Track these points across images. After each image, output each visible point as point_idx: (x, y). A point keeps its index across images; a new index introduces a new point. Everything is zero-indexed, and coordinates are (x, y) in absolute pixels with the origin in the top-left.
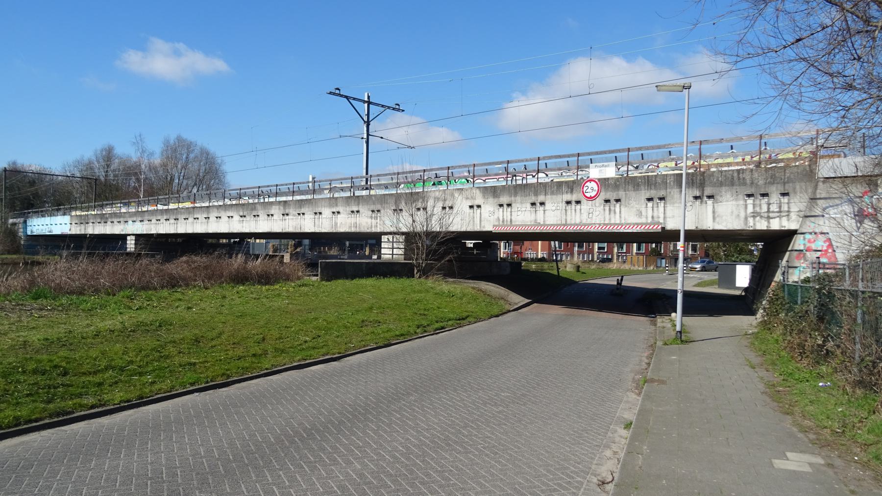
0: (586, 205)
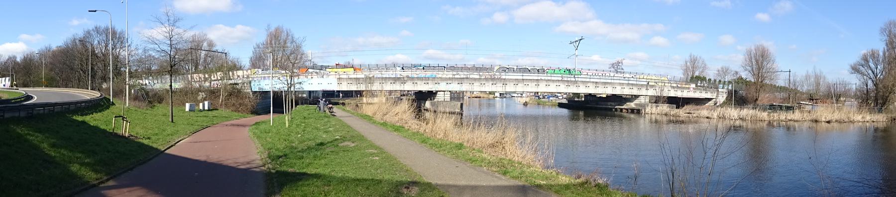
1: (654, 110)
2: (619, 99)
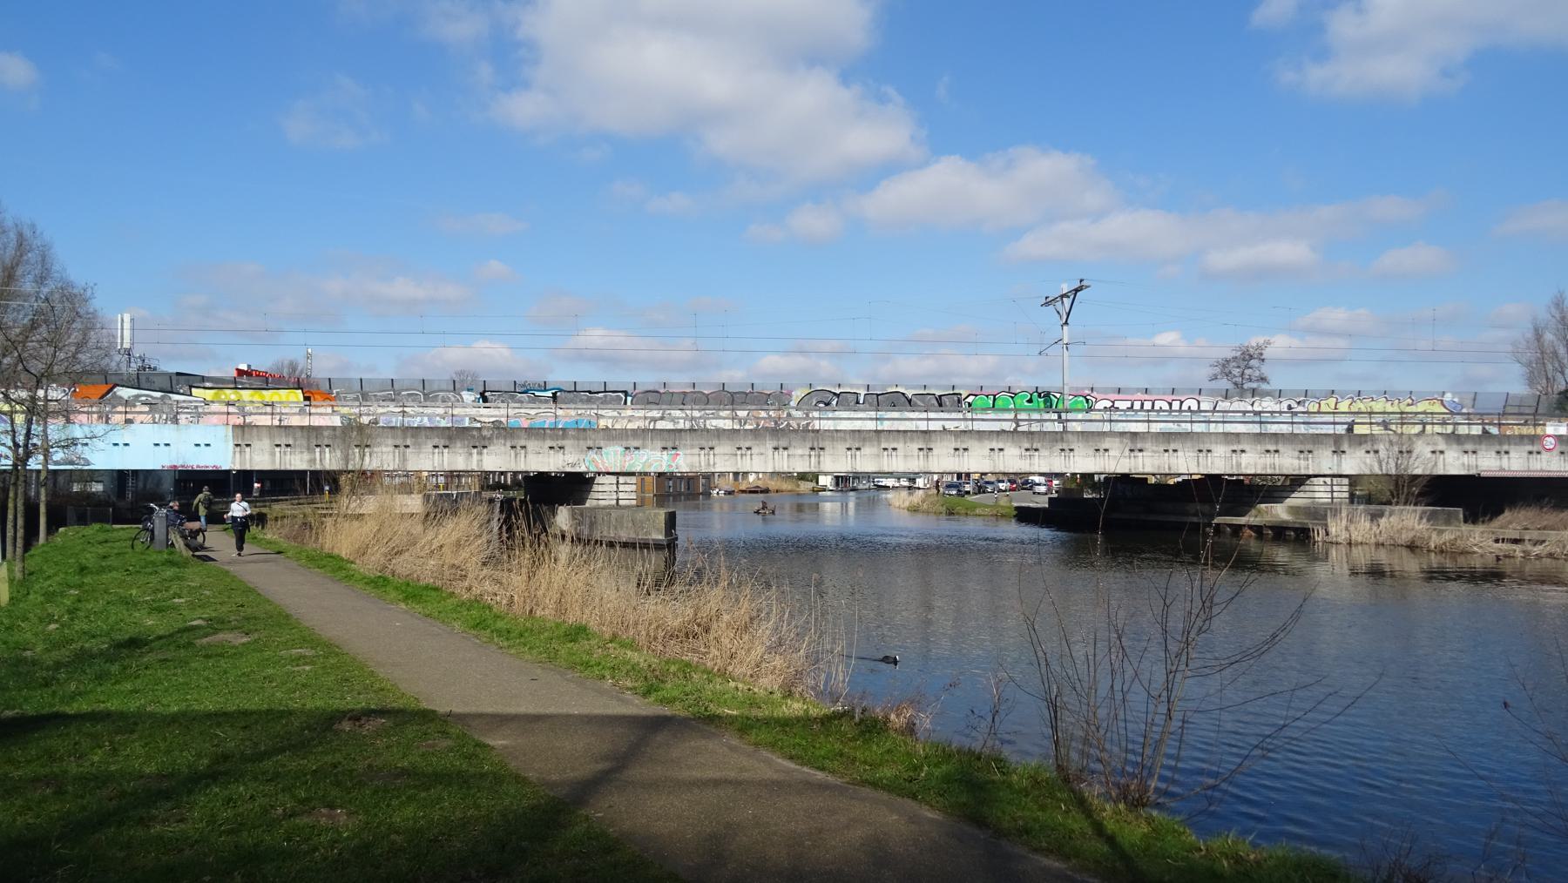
0: (1545, 456)
1: (1363, 528)
2: (1242, 492)
